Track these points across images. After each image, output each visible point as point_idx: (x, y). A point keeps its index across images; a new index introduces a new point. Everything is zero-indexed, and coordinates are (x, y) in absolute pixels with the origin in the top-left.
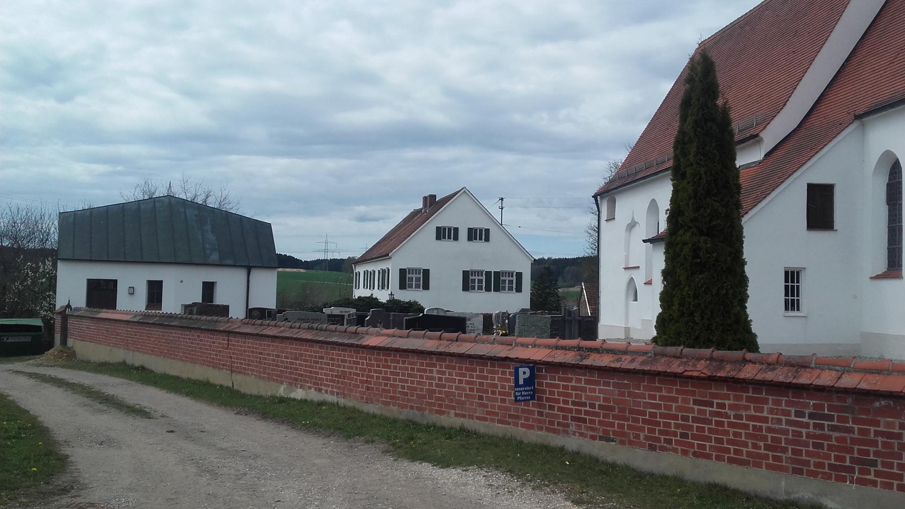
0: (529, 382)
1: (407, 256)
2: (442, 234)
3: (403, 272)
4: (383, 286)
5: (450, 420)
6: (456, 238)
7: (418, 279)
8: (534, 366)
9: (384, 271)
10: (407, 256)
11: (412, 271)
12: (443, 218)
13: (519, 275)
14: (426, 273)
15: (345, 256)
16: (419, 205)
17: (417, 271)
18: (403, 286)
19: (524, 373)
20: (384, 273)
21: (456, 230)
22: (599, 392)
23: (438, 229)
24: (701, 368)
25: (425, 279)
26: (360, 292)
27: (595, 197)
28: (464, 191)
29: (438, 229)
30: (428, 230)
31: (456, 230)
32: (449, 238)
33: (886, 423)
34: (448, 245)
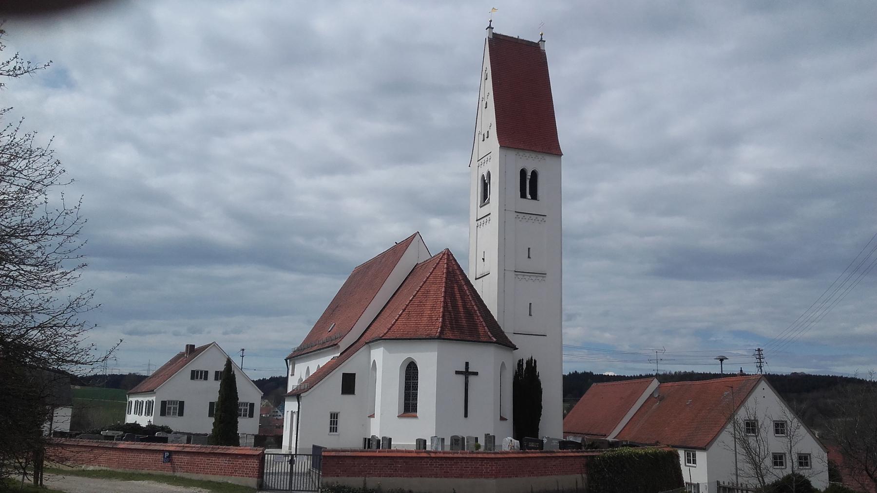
0: (168, 457)
1: (170, 391)
2: (195, 375)
3: (164, 404)
4: (149, 413)
5: (145, 471)
6: (206, 378)
7: (175, 409)
8: (170, 452)
9: (150, 402)
10: (170, 391)
11: (171, 402)
12: (198, 364)
13: (252, 405)
14: (182, 404)
15: (125, 372)
16: (184, 350)
17: (174, 402)
18: (163, 413)
19: (167, 454)
20: (150, 404)
21: (206, 372)
22: (186, 458)
23: (193, 372)
24: (208, 451)
25: (181, 409)
26: (131, 418)
27: (286, 360)
28: (214, 344)
29: (193, 372)
30: (186, 372)
31: (206, 372)
32: (201, 378)
33: (240, 461)
34: (199, 384)
